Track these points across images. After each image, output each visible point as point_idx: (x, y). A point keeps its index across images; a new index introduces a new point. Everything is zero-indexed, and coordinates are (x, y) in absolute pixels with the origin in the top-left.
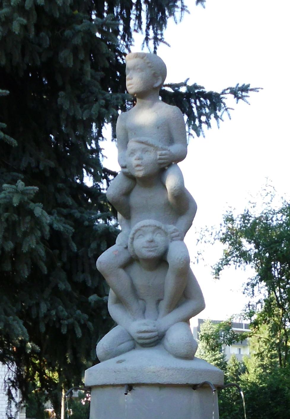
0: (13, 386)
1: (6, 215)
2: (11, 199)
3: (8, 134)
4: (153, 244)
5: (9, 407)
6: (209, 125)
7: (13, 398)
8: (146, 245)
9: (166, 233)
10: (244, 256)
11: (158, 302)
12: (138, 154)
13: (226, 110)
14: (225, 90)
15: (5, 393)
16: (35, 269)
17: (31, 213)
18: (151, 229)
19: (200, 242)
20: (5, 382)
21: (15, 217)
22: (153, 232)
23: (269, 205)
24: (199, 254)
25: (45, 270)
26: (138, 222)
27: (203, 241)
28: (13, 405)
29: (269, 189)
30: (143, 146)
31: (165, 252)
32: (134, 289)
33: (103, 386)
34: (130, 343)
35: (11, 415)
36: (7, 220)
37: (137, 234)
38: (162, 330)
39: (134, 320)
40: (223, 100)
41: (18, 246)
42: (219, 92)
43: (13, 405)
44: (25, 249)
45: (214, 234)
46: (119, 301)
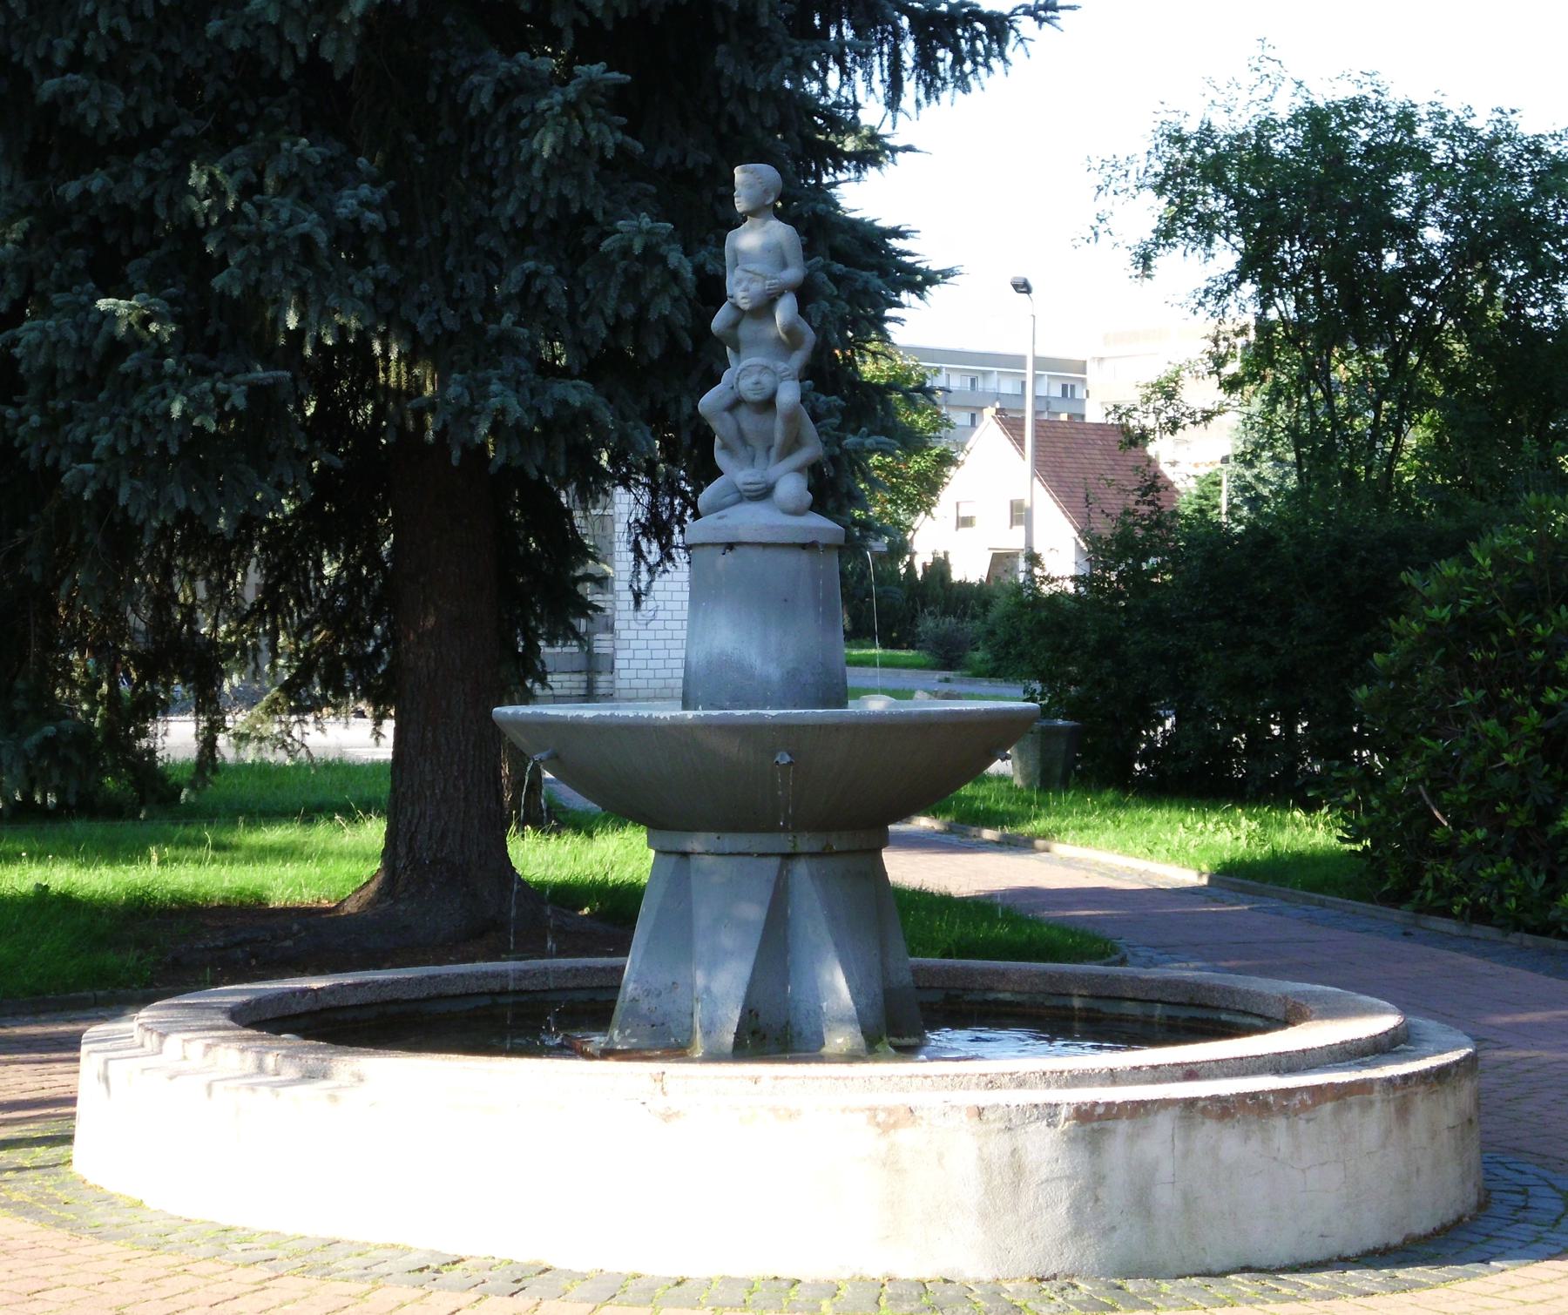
0: (644, 534)
1: (623, 264)
2: (631, 240)
3: (629, 135)
4: (759, 386)
5: (636, 573)
6: (990, 69)
7: (644, 558)
8: (751, 386)
9: (775, 373)
10: (1207, 226)
11: (769, 448)
12: (744, 284)
13: (1021, 40)
14: (1016, 9)
15: (629, 547)
16: (672, 344)
17: (663, 260)
18: (759, 369)
19: (1103, 192)
20: (629, 525)
21: (638, 267)
22: (760, 372)
23: (1266, 105)
24: (1101, 221)
25: (688, 344)
26: (746, 358)
27: (1110, 191)
28: (643, 567)
29: (1270, 68)
30: (750, 275)
31: (774, 394)
32: (741, 435)
33: (703, 545)
34: (736, 496)
35: (639, 588)
36: (625, 270)
37: (744, 373)
38: (771, 482)
39: (742, 469)
40: (1015, 25)
41: (643, 309)
42: (1007, 12)
43: (643, 567)
44: (653, 316)
45: (1132, 176)
46: (725, 447)
